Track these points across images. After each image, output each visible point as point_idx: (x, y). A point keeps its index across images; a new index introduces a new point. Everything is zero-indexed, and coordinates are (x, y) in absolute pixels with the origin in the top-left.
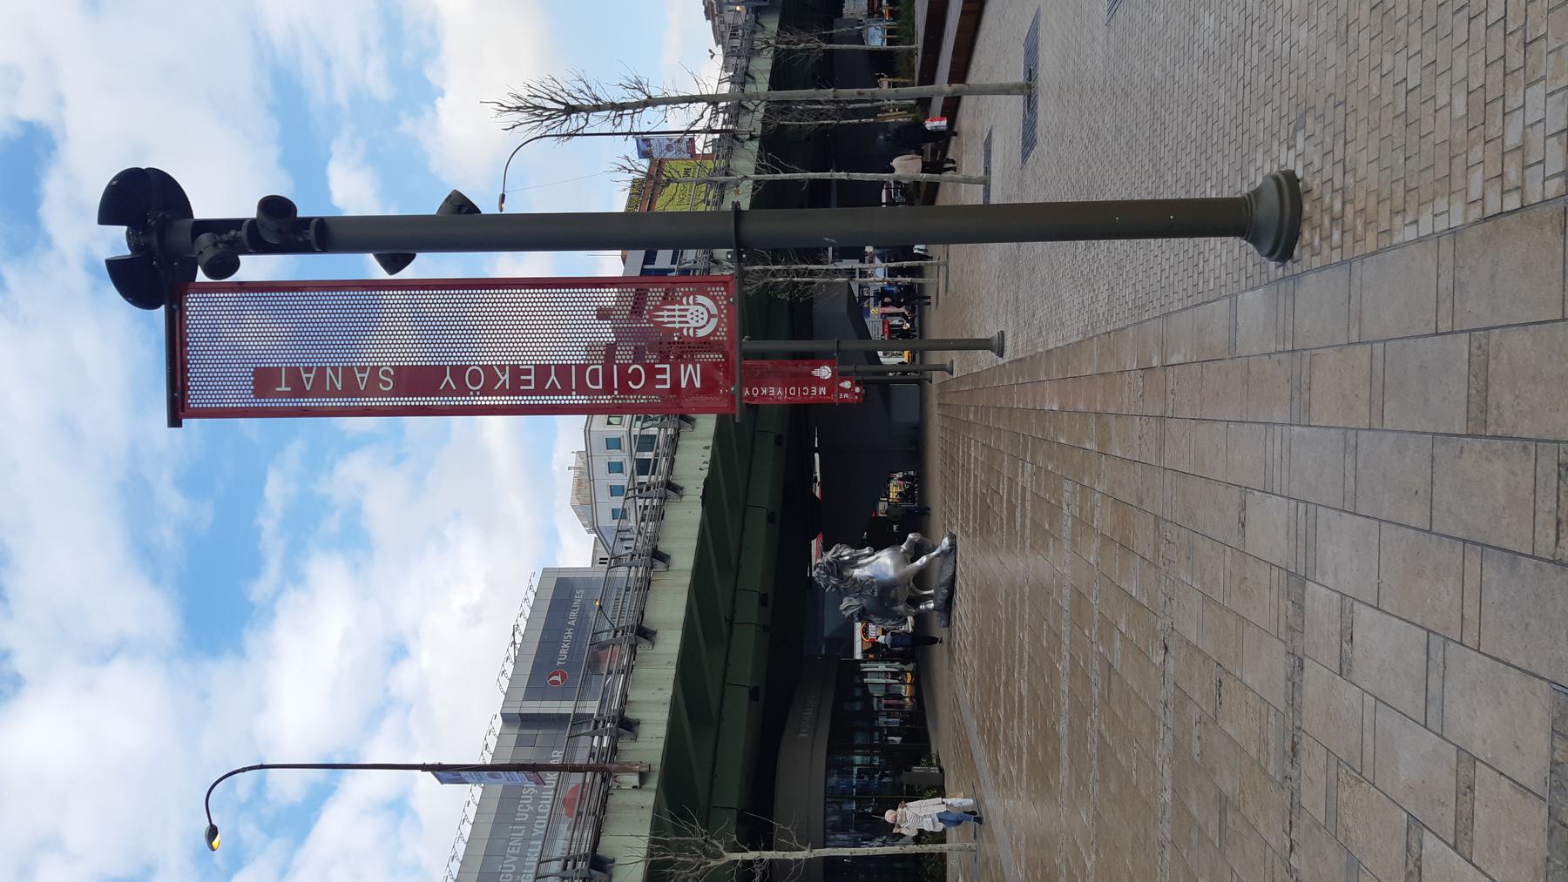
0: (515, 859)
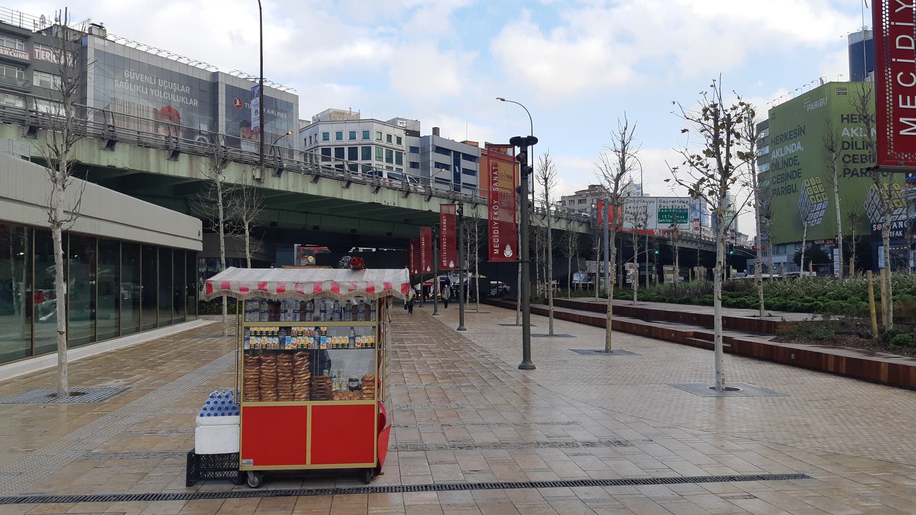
0: (137, 79)
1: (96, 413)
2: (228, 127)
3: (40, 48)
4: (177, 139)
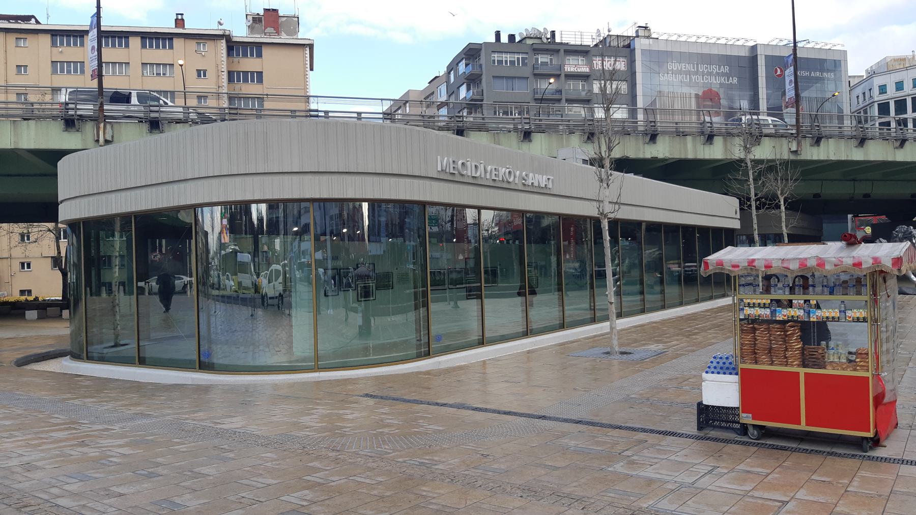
1: (637, 369)
2: (769, 99)
3: (598, 59)
4: (711, 123)
